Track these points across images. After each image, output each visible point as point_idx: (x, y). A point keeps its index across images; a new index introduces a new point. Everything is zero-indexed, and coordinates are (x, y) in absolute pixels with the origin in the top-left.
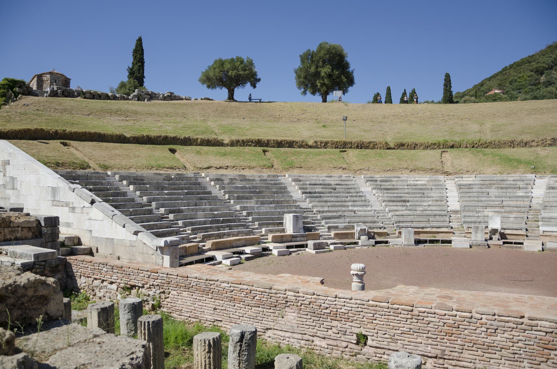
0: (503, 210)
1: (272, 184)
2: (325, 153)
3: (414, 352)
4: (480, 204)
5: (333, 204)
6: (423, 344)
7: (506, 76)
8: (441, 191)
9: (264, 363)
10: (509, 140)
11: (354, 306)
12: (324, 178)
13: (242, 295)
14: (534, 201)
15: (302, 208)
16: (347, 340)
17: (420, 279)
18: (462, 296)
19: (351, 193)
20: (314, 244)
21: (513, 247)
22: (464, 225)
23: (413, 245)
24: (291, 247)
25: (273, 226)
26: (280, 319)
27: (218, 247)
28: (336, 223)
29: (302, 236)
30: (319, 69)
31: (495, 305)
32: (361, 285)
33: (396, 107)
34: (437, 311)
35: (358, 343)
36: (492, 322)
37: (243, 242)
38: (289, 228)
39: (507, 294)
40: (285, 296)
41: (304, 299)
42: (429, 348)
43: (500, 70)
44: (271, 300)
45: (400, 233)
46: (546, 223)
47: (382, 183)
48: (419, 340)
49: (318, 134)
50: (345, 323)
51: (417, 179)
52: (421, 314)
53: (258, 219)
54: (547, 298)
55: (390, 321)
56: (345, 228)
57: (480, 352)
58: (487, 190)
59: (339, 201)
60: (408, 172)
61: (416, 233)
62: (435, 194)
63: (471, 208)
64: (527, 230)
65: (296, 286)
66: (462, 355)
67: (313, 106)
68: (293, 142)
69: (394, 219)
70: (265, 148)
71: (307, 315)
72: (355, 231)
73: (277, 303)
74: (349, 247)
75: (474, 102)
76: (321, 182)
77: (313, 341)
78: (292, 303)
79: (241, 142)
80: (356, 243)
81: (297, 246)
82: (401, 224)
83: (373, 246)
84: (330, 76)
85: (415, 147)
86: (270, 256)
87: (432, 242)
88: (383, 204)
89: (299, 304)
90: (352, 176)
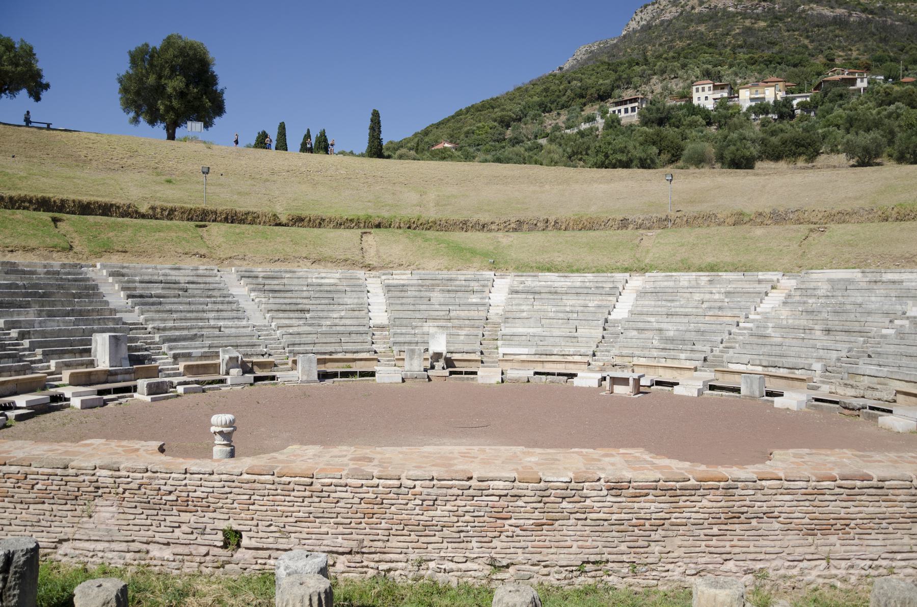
0: (450, 324)
1: (69, 280)
2: (169, 228)
3: (317, 548)
4: (418, 315)
5: (182, 315)
6: (330, 535)
7: (460, 125)
8: (361, 295)
9: (55, 604)
10: (461, 219)
11: (216, 484)
12: (167, 271)
13: (8, 484)
14: (493, 311)
15: (126, 324)
16: (207, 542)
17: (325, 436)
18: (387, 456)
19: (214, 297)
20: (149, 386)
21: (463, 379)
22: (394, 348)
23: (315, 382)
24: (108, 392)
25: (71, 355)
26: (85, 519)
28: (187, 348)
29: (127, 372)
30: (163, 81)
31: (433, 465)
32: (229, 449)
33: (294, 157)
34: (349, 481)
35: (225, 546)
36: (429, 490)
37: (11, 387)
38: (102, 359)
39: (450, 448)
40: (94, 478)
41: (129, 480)
42: (340, 540)
43: (453, 113)
44: (68, 488)
45: (295, 362)
46: (507, 342)
47: (267, 282)
48: (324, 529)
49: (158, 195)
50: (202, 514)
51: (323, 275)
52: (325, 488)
53: (40, 345)
54: (503, 448)
55: (277, 503)
56: (204, 356)
57: (413, 537)
58: (428, 294)
59: (192, 311)
60: (309, 264)
61: (320, 362)
62: (350, 300)
63: (405, 322)
64: (482, 353)
65: (115, 458)
66: (388, 544)
67: (150, 144)
68: (112, 205)
69: (286, 340)
70: (57, 215)
71: (136, 507)
72: (220, 361)
73: (79, 493)
74: (209, 389)
75: (414, 159)
76: (161, 278)
77: (148, 552)
78: (107, 490)
79: (7, 200)
80: (222, 381)
81: (117, 391)
82: (296, 348)
83: (251, 384)
84: (182, 95)
85: (320, 224)
86: (67, 410)
87: (345, 375)
88: (268, 315)
89: (121, 490)
90: (216, 268)
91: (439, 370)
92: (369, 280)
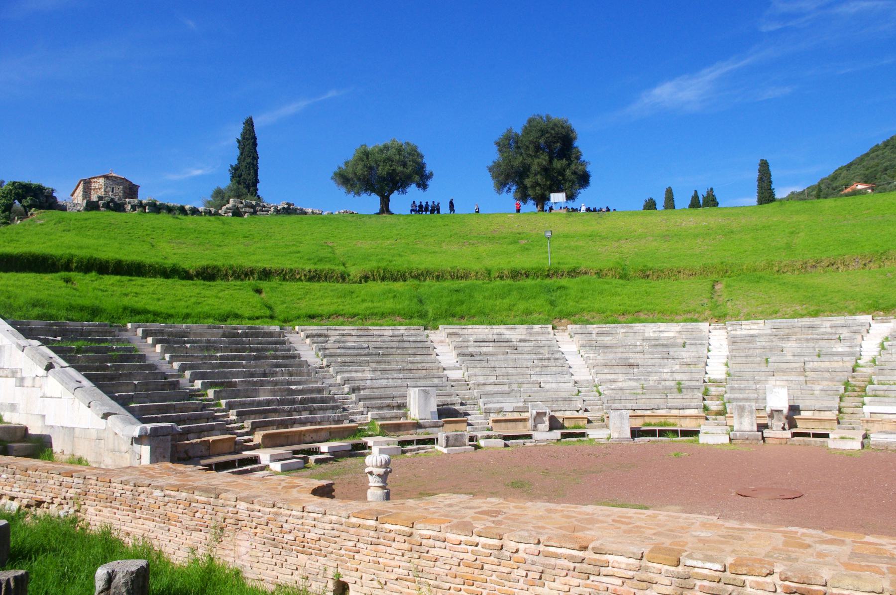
23: (627, 439)
27: (270, 442)
37: (324, 435)
43: (867, 151)
58: (780, 344)
89: (254, 524)
91: (777, 432)
92: (714, 332)
